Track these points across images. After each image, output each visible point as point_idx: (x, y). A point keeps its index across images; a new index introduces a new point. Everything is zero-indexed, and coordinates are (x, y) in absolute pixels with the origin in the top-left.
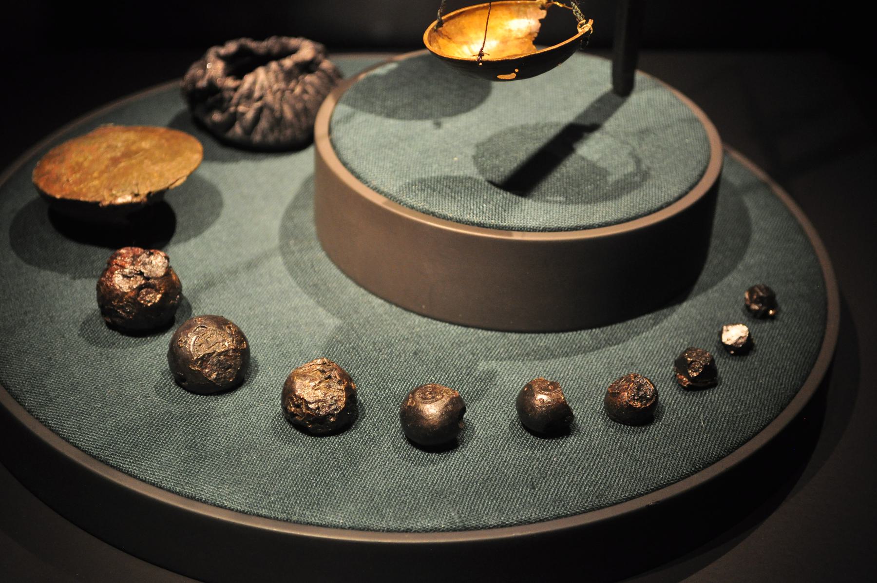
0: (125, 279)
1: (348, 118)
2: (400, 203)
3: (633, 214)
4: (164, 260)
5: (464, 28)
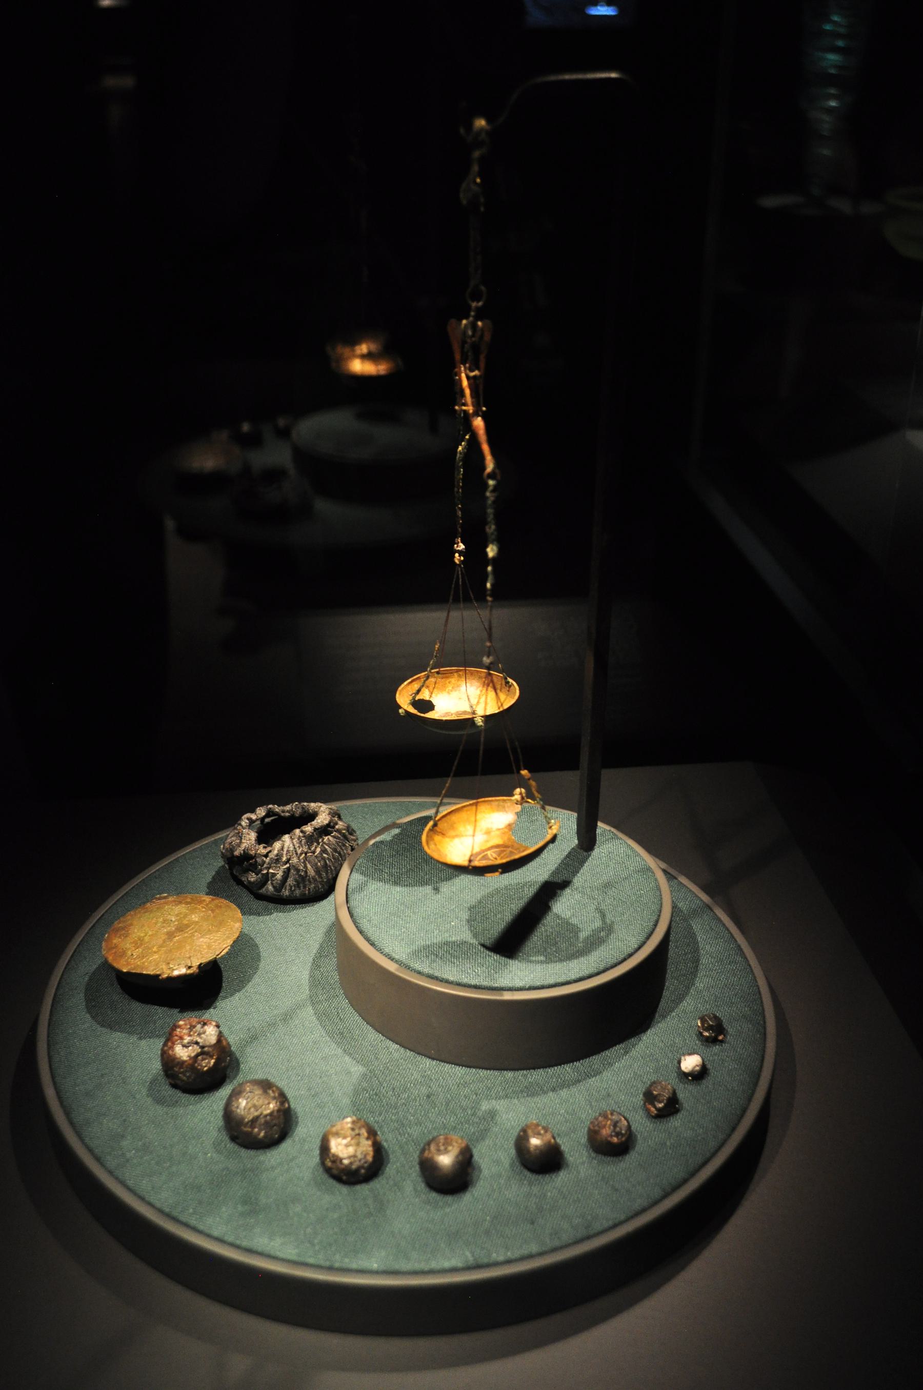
0: (184, 1048)
1: (361, 888)
2: (409, 969)
3: (601, 968)
4: (216, 1029)
5: (455, 823)
